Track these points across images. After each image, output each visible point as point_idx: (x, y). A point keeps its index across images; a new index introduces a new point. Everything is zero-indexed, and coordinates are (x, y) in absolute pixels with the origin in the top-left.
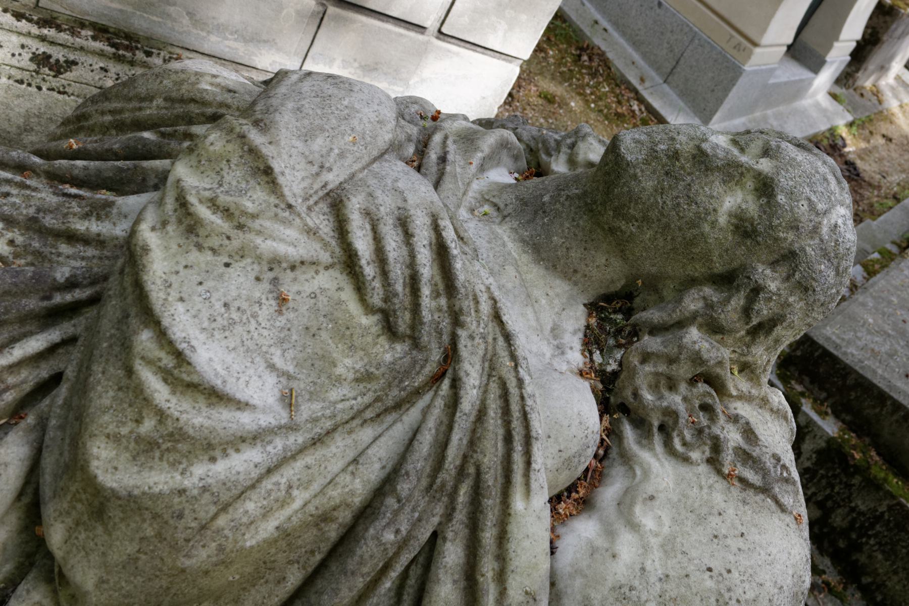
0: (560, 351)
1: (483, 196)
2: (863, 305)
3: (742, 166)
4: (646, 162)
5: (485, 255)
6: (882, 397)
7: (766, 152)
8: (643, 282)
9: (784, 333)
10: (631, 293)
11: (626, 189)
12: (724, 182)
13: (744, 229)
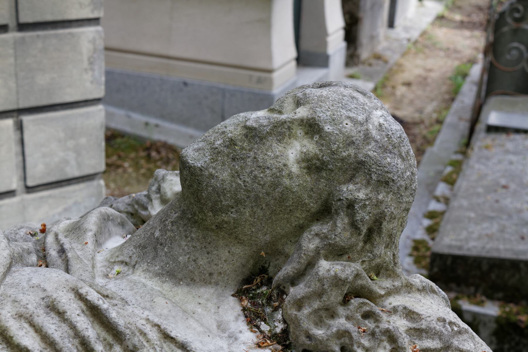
0: (233, 339)
1: (109, 261)
2: (461, 207)
3: (285, 122)
4: (214, 160)
5: (134, 301)
6: (514, 265)
7: (298, 103)
8: (266, 253)
9: (391, 226)
10: (263, 267)
11: (210, 189)
12: (279, 141)
13: (313, 166)
